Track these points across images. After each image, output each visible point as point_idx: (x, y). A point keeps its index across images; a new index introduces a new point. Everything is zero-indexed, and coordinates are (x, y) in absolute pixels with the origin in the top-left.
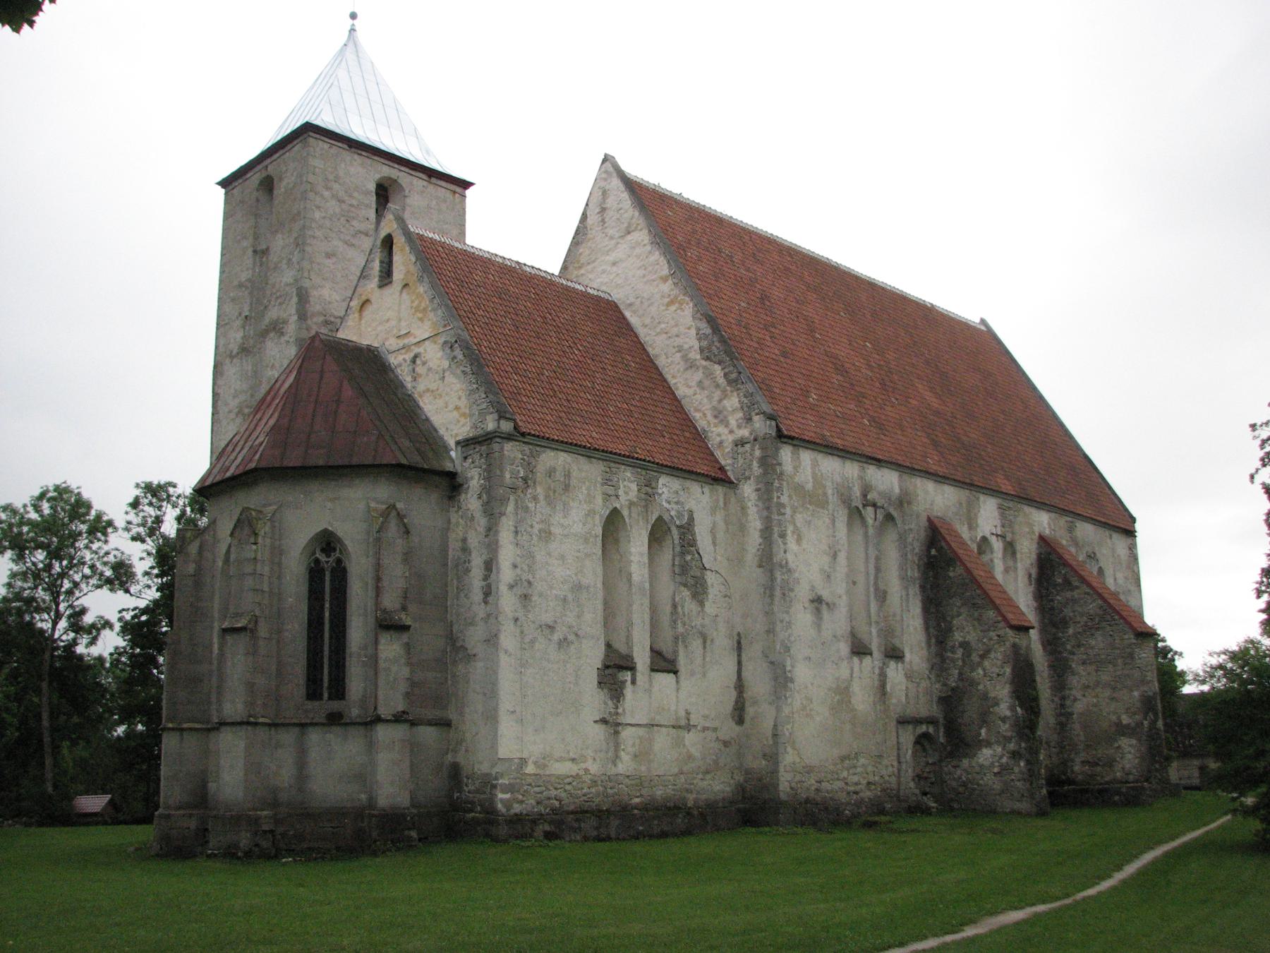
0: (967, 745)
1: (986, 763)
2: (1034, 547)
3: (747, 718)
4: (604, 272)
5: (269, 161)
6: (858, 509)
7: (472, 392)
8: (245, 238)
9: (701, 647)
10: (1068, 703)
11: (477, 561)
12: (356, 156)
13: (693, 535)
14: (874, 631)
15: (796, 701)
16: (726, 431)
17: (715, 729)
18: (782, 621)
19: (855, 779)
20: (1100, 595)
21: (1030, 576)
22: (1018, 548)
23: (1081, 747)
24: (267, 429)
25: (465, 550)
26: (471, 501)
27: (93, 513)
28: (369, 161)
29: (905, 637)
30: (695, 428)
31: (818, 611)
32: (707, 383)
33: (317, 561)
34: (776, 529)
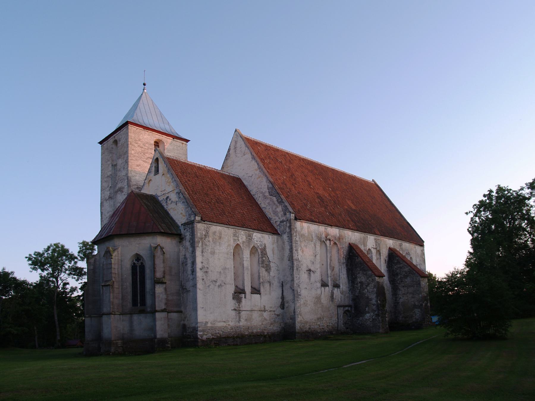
2: (388, 251)
3: (285, 307)
6: (324, 240)
7: (186, 208)
8: (109, 161)
11: (189, 262)
13: (266, 251)
14: (329, 279)
15: (301, 301)
17: (274, 311)
22: (381, 252)
25: (185, 258)
26: (187, 244)
27: (484, 199)
28: (151, 134)
29: (341, 280)
32: (271, 203)
33: (134, 263)
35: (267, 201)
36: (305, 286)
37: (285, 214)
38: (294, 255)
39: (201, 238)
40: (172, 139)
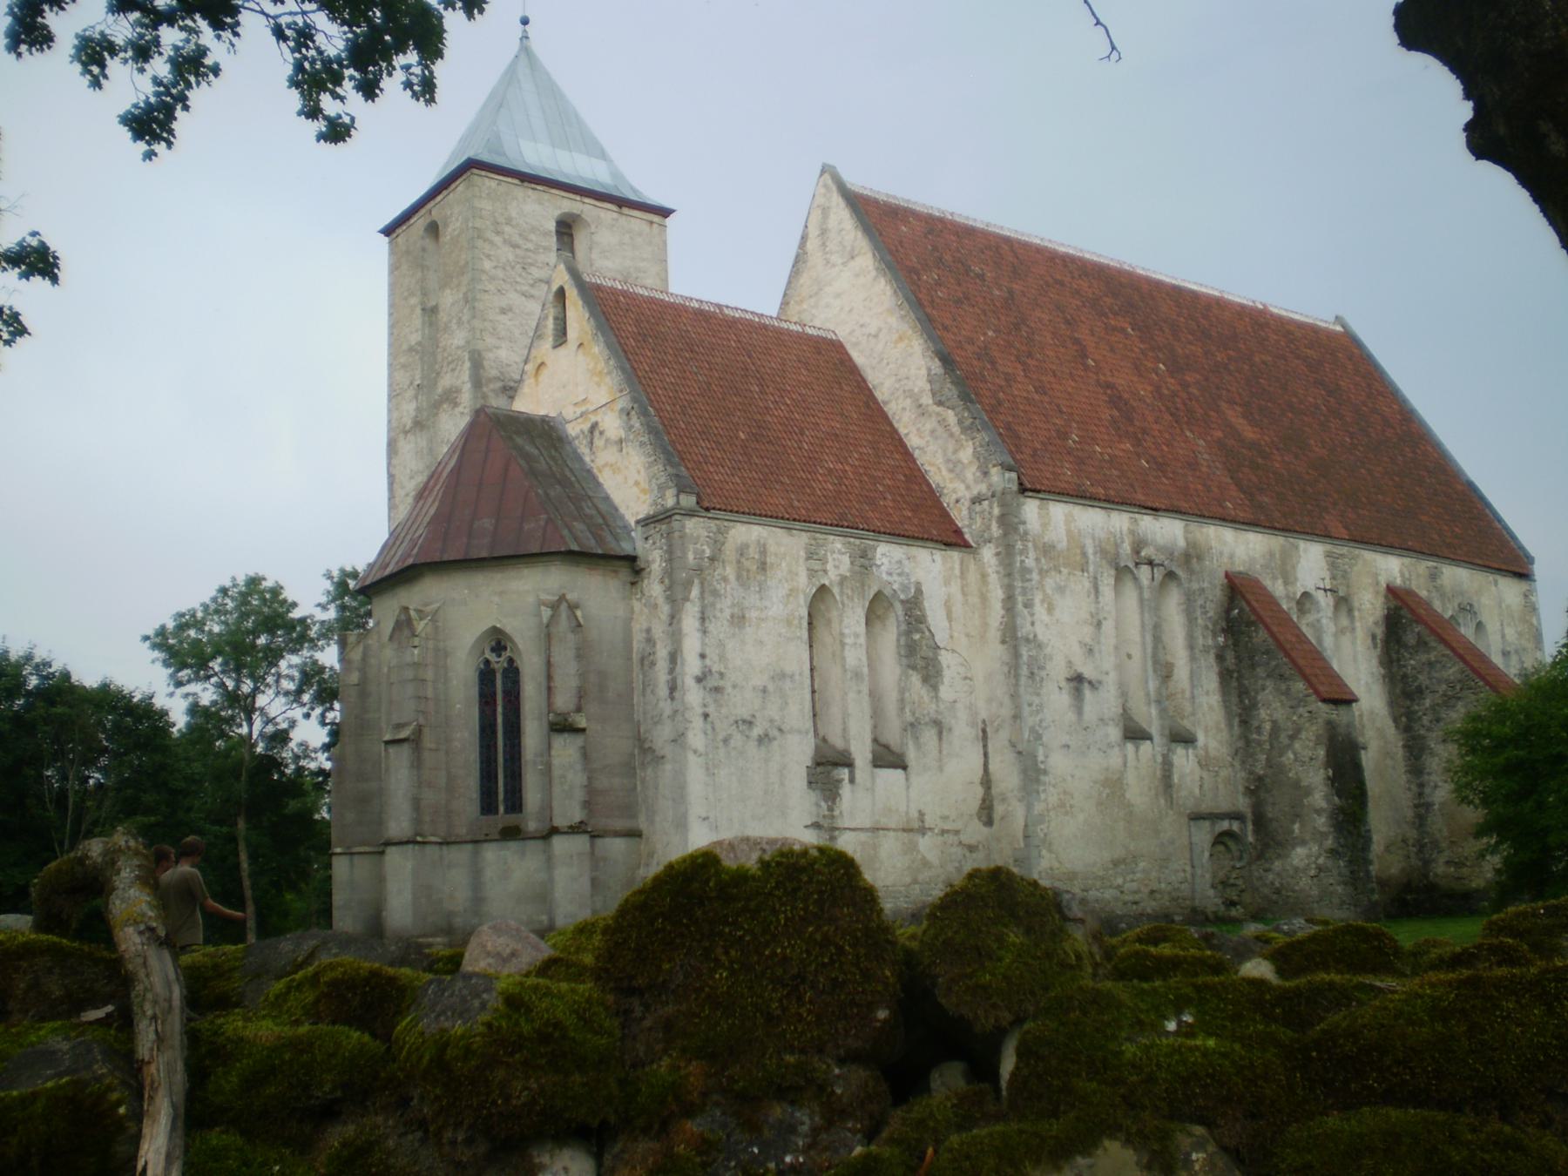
0: (1279, 844)
1: (1301, 865)
2: (1381, 600)
4: (827, 306)
5: (432, 203)
7: (650, 465)
8: (412, 294)
9: (935, 738)
10: (1427, 790)
11: (662, 653)
12: (530, 192)
16: (962, 487)
17: (957, 832)
18: (1030, 705)
19: (1134, 886)
20: (1461, 658)
21: (1374, 637)
22: (1356, 604)
23: (1444, 845)
24: (427, 519)
25: (650, 641)
26: (654, 588)
28: (546, 196)
30: (929, 485)
31: (1078, 694)
32: (940, 430)
33: (487, 662)
34: (1020, 599)
35: (928, 426)
36: (1065, 739)
37: (986, 474)
38: (1019, 621)
39: (699, 570)
40: (614, 207)
